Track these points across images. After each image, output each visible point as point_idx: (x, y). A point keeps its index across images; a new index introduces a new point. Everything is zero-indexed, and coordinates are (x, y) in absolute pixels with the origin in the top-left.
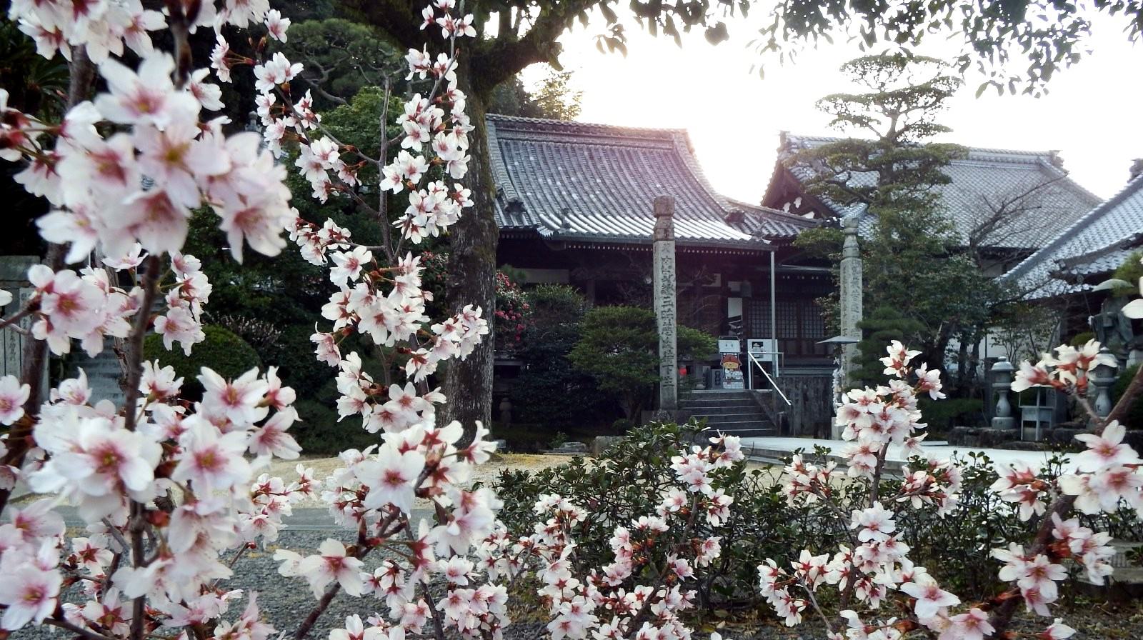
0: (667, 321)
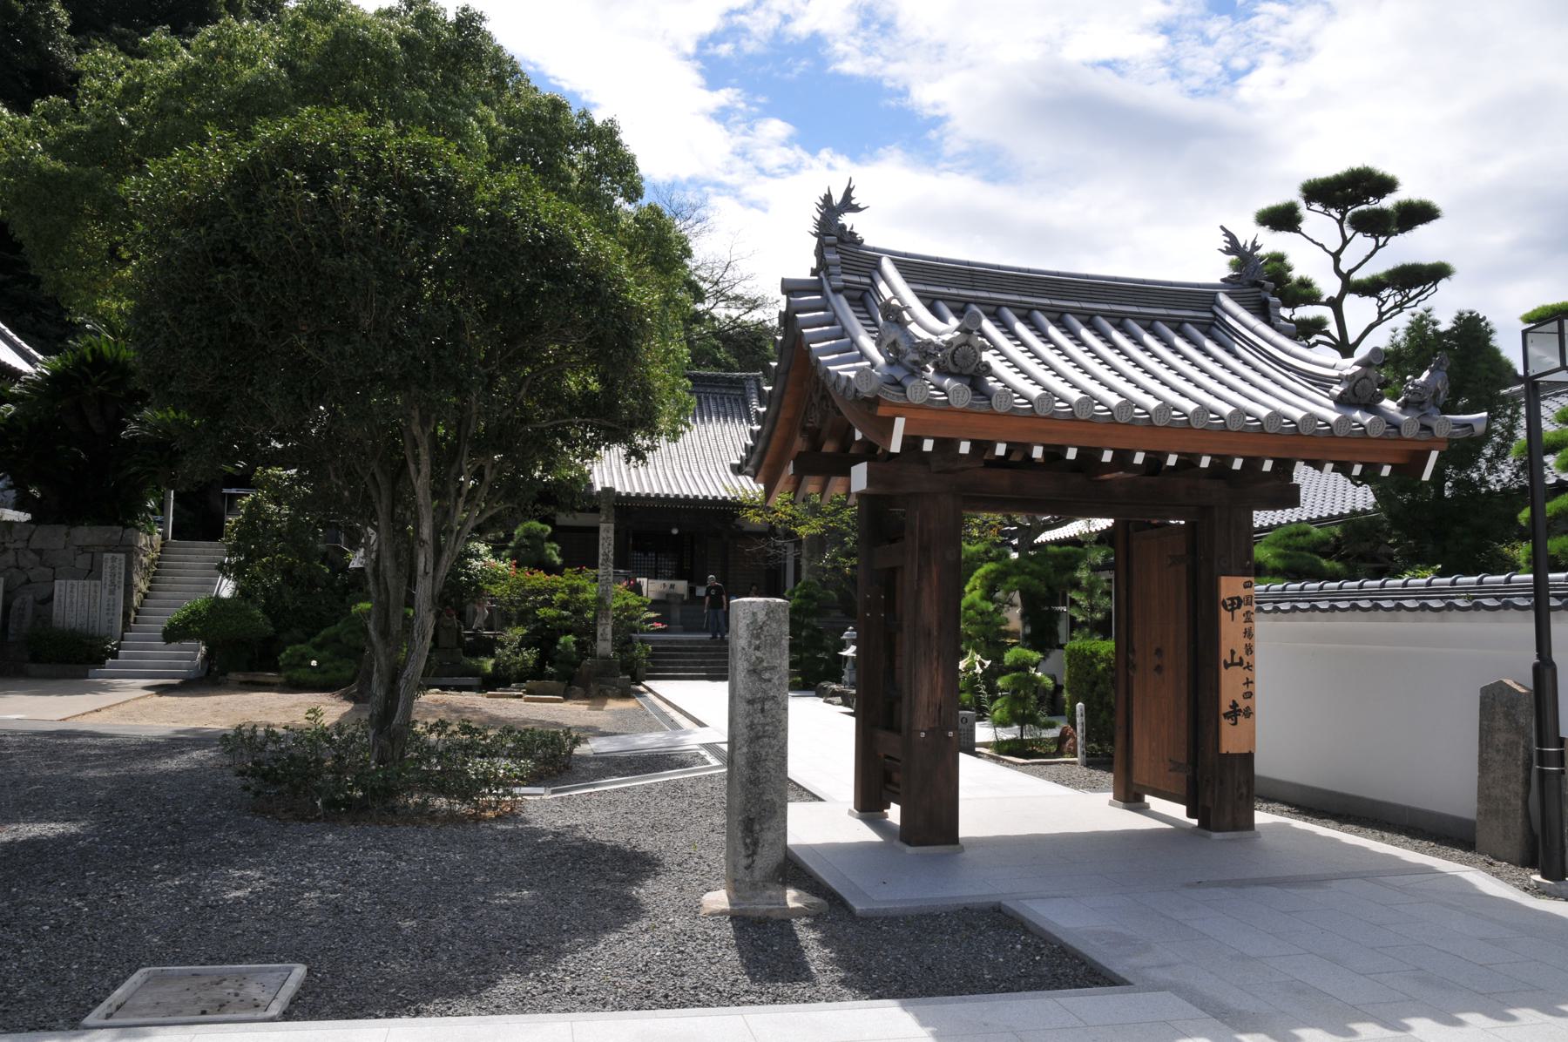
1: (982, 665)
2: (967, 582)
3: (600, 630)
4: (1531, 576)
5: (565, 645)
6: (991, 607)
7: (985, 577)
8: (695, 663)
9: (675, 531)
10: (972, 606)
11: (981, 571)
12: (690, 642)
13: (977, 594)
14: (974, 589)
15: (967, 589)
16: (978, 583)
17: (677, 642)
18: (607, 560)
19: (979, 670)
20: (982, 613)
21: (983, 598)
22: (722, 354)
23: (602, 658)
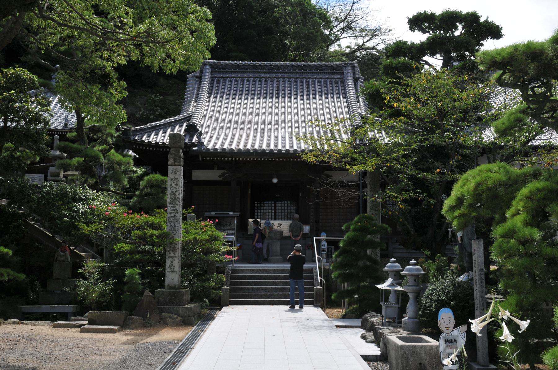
0: (173, 224)
1: (513, 328)
2: (509, 206)
3: (168, 263)
4: (290, 265)
5: (131, 277)
6: (537, 235)
7: (529, 198)
8: (276, 290)
9: (275, 181)
10: (510, 234)
11: (525, 191)
12: (275, 271)
13: (519, 221)
14: (517, 213)
15: (509, 214)
16: (521, 206)
17: (264, 271)
18: (174, 199)
19: (507, 335)
20: (524, 242)
21: (527, 224)
22: (343, 58)
23: (170, 287)
